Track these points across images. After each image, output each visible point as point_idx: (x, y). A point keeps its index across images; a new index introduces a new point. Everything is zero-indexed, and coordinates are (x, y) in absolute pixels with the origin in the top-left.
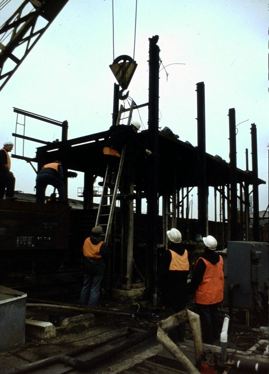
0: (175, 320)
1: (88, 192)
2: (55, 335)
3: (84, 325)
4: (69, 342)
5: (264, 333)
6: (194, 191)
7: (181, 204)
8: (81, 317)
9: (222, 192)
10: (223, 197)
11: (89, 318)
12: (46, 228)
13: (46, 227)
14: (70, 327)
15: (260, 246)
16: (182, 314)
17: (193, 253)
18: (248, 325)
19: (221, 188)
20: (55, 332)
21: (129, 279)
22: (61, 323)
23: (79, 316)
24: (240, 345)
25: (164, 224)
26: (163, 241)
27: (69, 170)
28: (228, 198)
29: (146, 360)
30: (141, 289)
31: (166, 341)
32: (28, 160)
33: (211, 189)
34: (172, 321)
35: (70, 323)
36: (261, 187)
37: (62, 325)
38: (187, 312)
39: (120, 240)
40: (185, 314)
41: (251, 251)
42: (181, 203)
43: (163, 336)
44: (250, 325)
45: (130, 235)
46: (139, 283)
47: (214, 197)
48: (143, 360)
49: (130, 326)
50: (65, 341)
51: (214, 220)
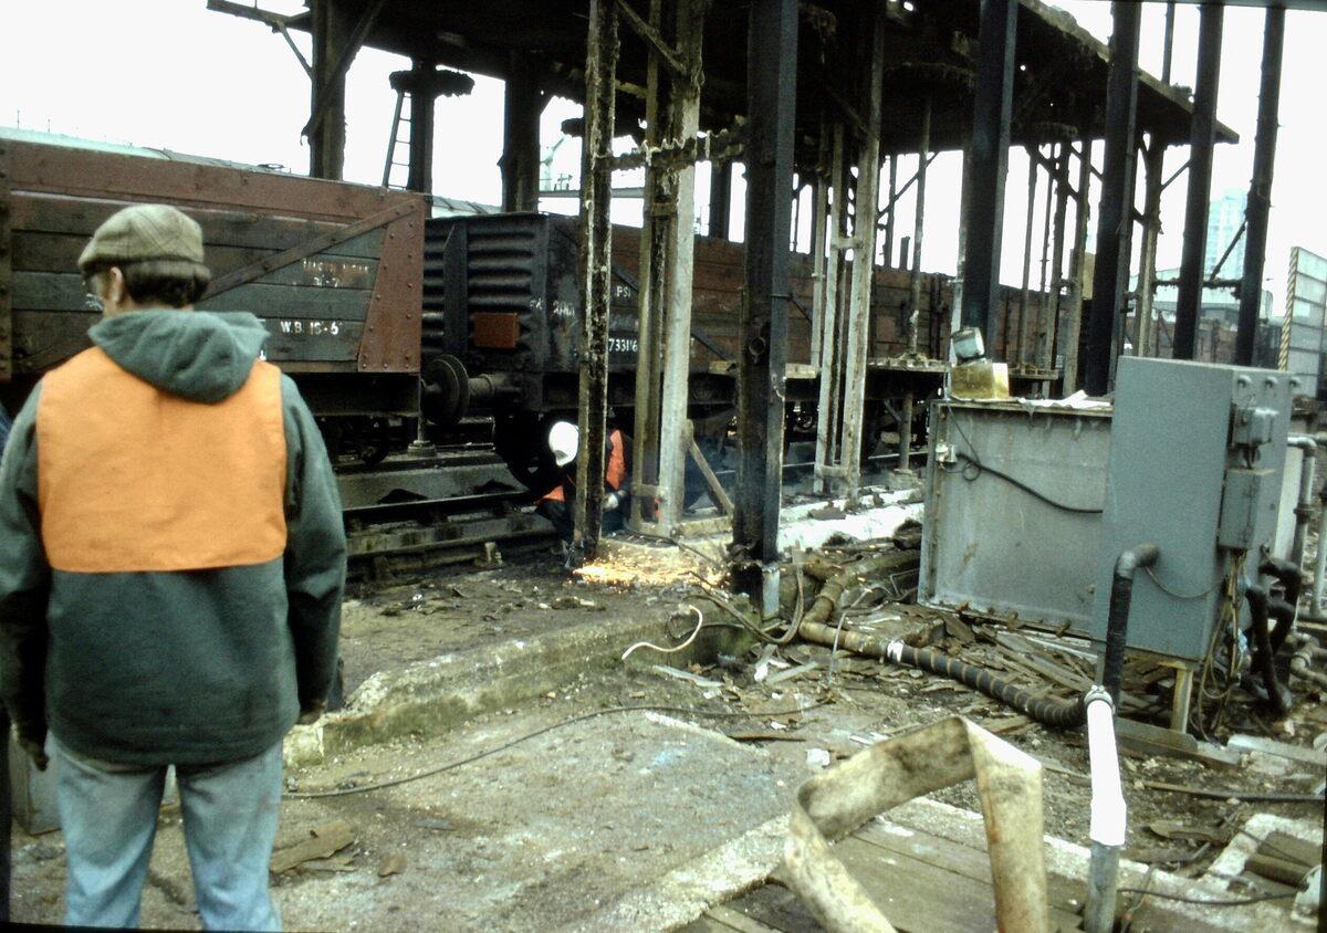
0: (888, 769)
1: (520, 159)
2: (321, 749)
3: (455, 703)
4: (381, 781)
5: (1252, 767)
6: (949, 167)
7: (883, 220)
8: (444, 666)
9: (1059, 173)
10: (1064, 190)
11: (480, 669)
12: (319, 284)
13: (318, 281)
14: (392, 711)
15: (1269, 383)
16: (932, 746)
17: (940, 405)
18: (1184, 731)
19: (1057, 155)
20: (321, 738)
21: (670, 500)
22: (351, 697)
23: (433, 664)
24: (1158, 826)
25: (817, 287)
26: (809, 351)
27: (440, 68)
28: (1134, 215)
29: (723, 903)
30: (716, 542)
31: (832, 894)
32: (277, 23)
33: (1018, 156)
34: (874, 779)
35: (389, 697)
36: (1220, 150)
37: (356, 706)
38: (964, 735)
39: (1319, 552)
40: (950, 748)
41: (1233, 406)
42: (886, 215)
43: (821, 866)
44: (1190, 730)
45: (677, 325)
46: (709, 516)
47: (1027, 188)
48: (703, 905)
49: (658, 705)
50: (359, 780)
51: (1020, 287)
